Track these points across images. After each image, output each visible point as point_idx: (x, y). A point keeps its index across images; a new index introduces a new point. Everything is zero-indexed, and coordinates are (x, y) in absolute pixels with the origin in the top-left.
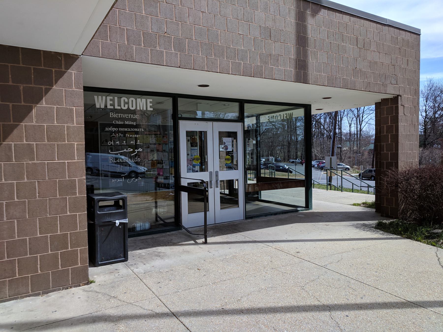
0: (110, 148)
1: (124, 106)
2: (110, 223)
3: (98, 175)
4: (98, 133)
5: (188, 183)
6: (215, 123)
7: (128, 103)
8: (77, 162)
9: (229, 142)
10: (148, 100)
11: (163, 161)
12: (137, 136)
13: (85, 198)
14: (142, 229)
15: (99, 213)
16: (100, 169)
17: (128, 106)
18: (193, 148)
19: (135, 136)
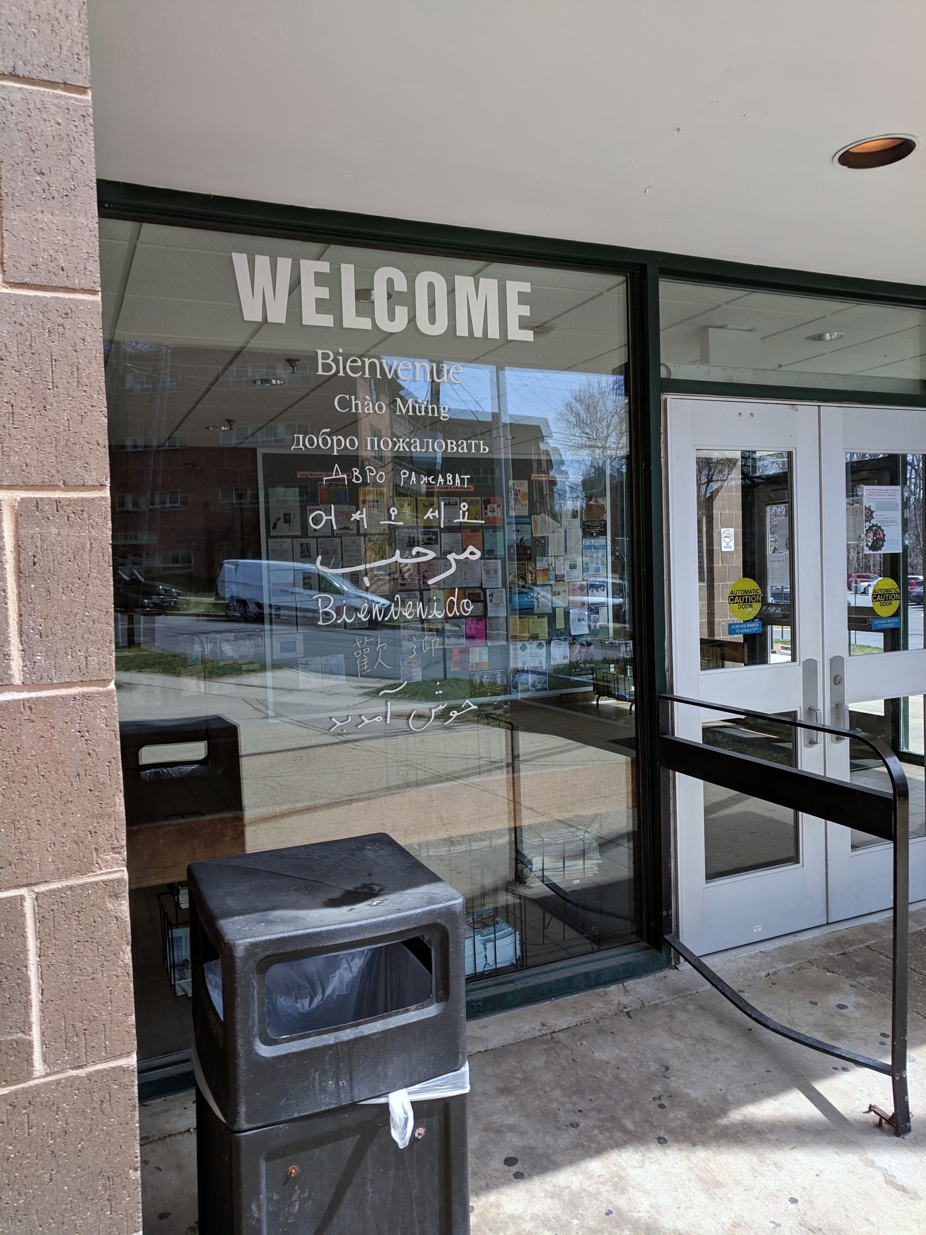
0: (302, 544)
1: (392, 316)
2: (348, 1119)
3: (259, 619)
4: (258, 503)
5: (706, 730)
6: (831, 411)
7: (409, 299)
8: (29, 705)
9: (888, 507)
10: (509, 284)
11: (484, 590)
12: (458, 481)
13: (126, 1087)
14: (480, 969)
15: (265, 1051)
16: (266, 602)
17: (412, 319)
18: (587, 542)
19: (445, 478)
